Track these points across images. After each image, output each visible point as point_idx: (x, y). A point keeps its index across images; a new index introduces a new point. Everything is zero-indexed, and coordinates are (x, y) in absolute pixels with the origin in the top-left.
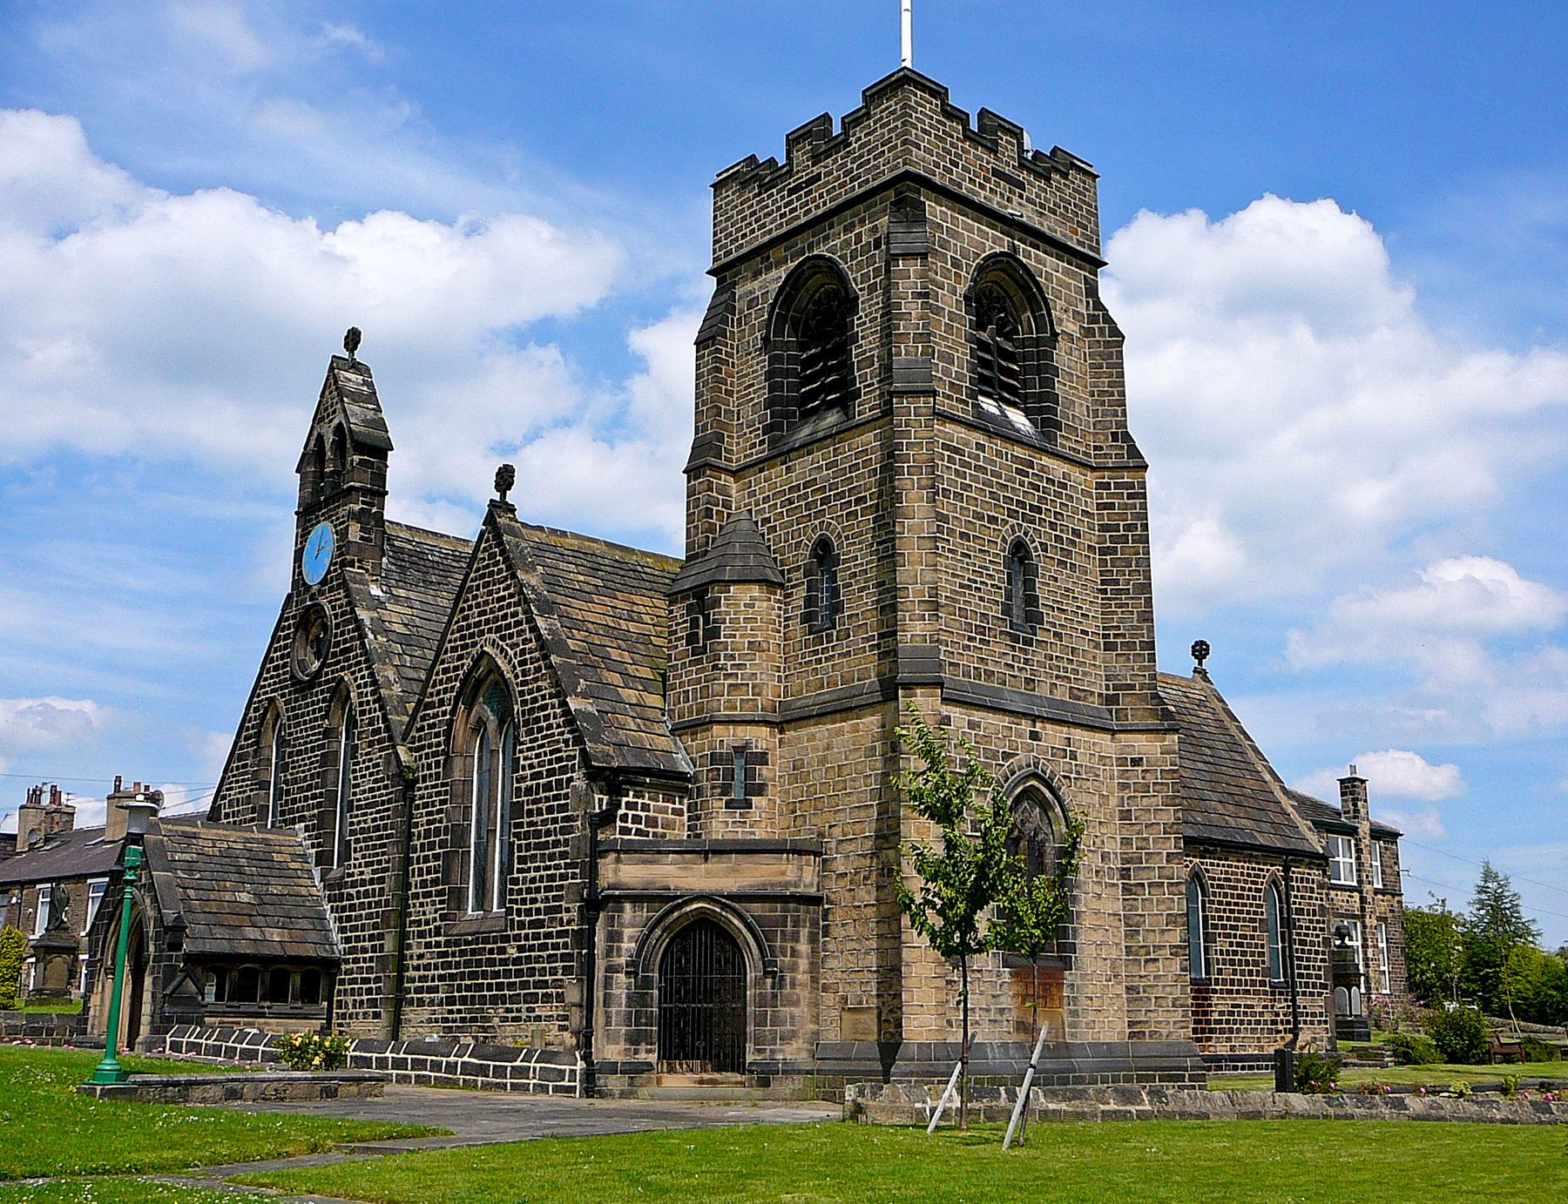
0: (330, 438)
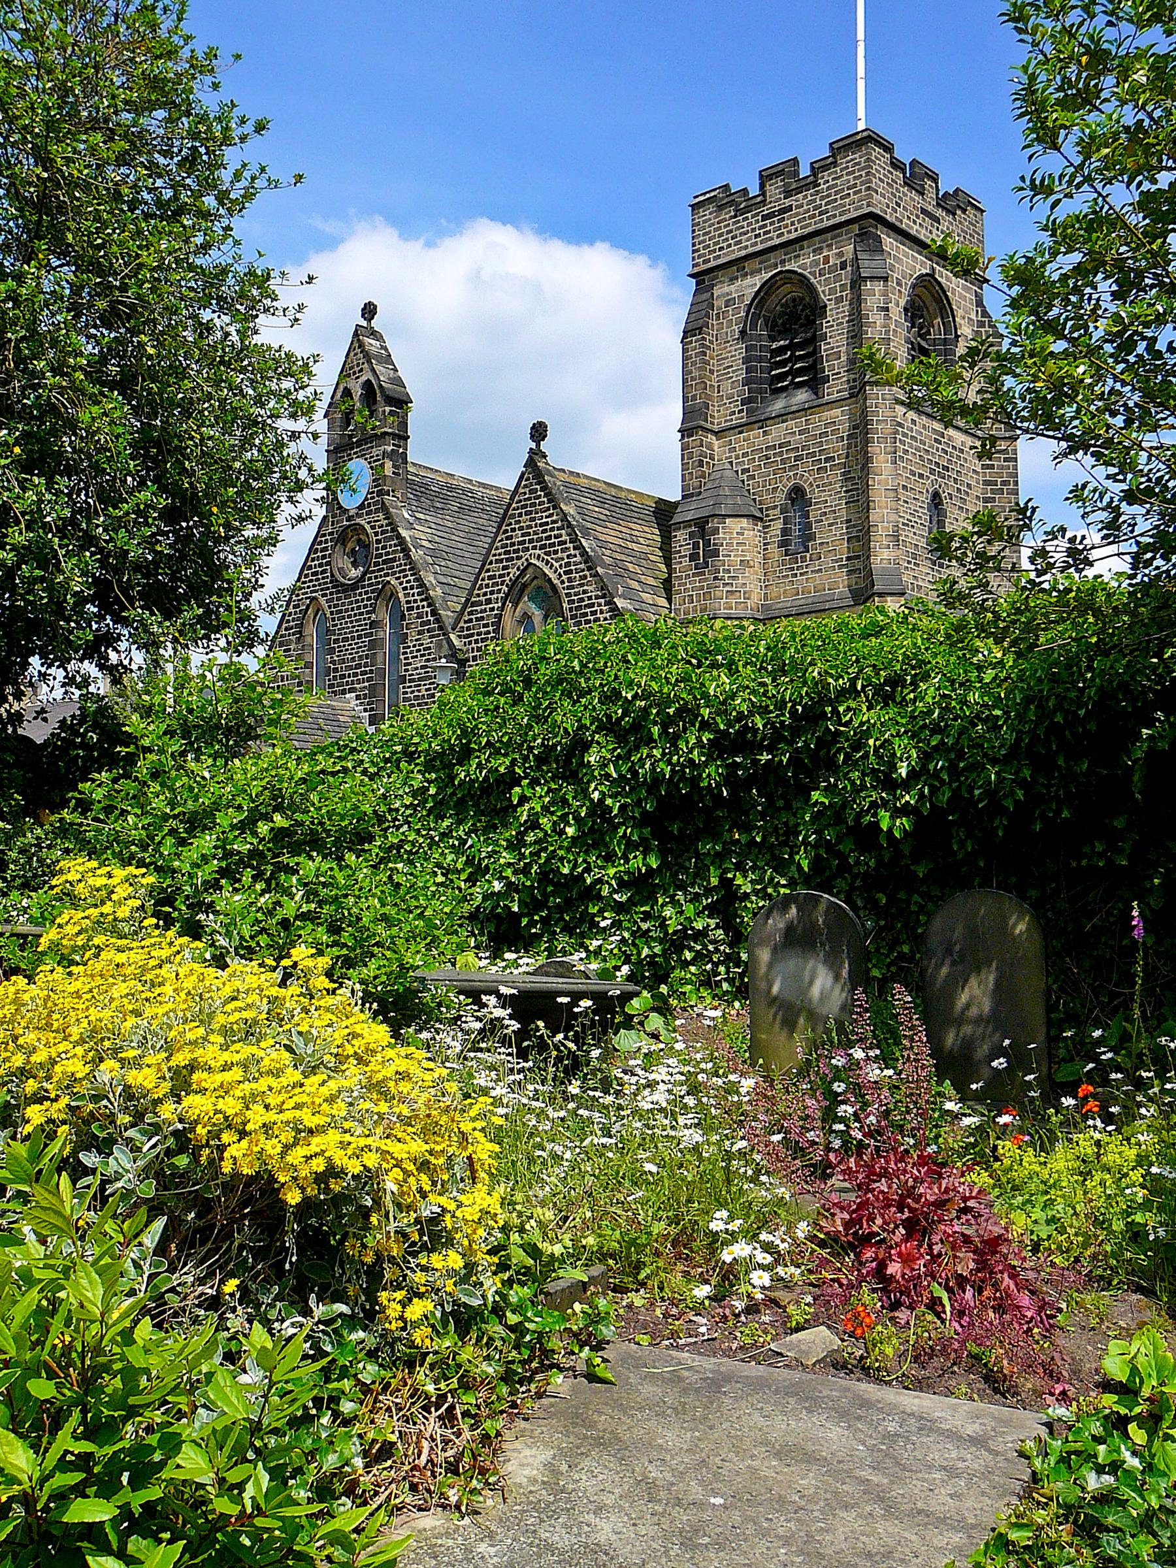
0: (357, 391)
